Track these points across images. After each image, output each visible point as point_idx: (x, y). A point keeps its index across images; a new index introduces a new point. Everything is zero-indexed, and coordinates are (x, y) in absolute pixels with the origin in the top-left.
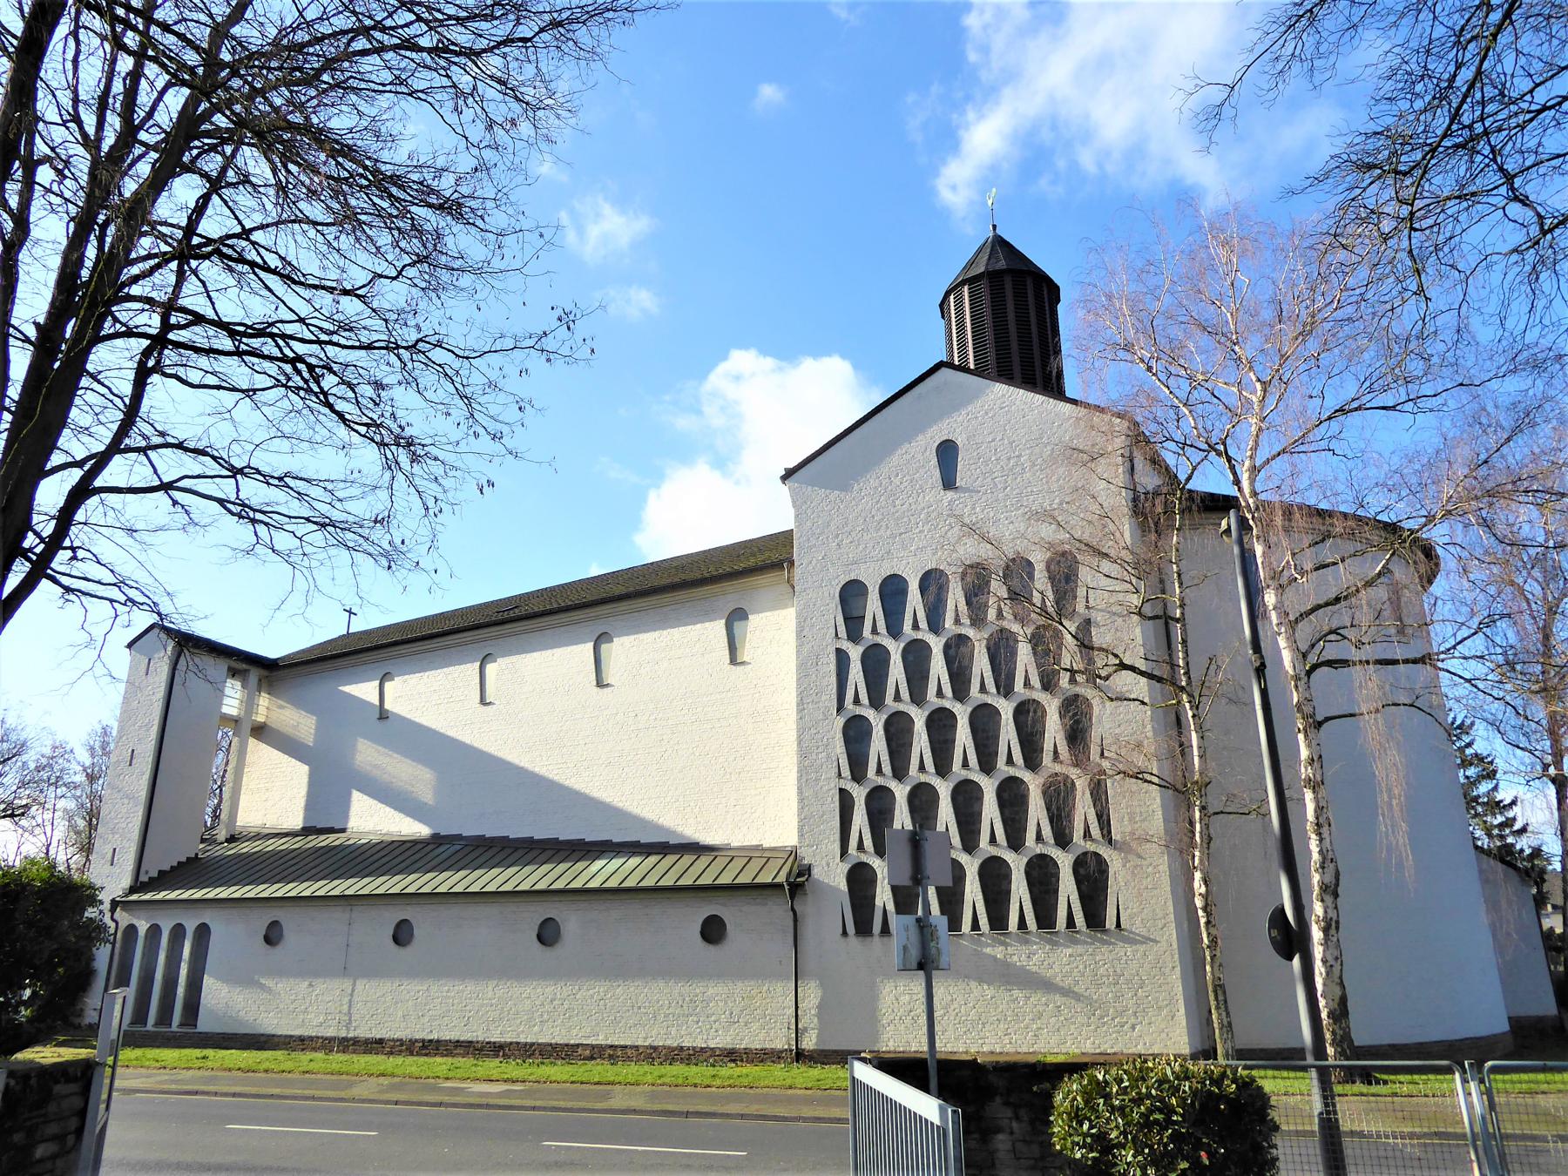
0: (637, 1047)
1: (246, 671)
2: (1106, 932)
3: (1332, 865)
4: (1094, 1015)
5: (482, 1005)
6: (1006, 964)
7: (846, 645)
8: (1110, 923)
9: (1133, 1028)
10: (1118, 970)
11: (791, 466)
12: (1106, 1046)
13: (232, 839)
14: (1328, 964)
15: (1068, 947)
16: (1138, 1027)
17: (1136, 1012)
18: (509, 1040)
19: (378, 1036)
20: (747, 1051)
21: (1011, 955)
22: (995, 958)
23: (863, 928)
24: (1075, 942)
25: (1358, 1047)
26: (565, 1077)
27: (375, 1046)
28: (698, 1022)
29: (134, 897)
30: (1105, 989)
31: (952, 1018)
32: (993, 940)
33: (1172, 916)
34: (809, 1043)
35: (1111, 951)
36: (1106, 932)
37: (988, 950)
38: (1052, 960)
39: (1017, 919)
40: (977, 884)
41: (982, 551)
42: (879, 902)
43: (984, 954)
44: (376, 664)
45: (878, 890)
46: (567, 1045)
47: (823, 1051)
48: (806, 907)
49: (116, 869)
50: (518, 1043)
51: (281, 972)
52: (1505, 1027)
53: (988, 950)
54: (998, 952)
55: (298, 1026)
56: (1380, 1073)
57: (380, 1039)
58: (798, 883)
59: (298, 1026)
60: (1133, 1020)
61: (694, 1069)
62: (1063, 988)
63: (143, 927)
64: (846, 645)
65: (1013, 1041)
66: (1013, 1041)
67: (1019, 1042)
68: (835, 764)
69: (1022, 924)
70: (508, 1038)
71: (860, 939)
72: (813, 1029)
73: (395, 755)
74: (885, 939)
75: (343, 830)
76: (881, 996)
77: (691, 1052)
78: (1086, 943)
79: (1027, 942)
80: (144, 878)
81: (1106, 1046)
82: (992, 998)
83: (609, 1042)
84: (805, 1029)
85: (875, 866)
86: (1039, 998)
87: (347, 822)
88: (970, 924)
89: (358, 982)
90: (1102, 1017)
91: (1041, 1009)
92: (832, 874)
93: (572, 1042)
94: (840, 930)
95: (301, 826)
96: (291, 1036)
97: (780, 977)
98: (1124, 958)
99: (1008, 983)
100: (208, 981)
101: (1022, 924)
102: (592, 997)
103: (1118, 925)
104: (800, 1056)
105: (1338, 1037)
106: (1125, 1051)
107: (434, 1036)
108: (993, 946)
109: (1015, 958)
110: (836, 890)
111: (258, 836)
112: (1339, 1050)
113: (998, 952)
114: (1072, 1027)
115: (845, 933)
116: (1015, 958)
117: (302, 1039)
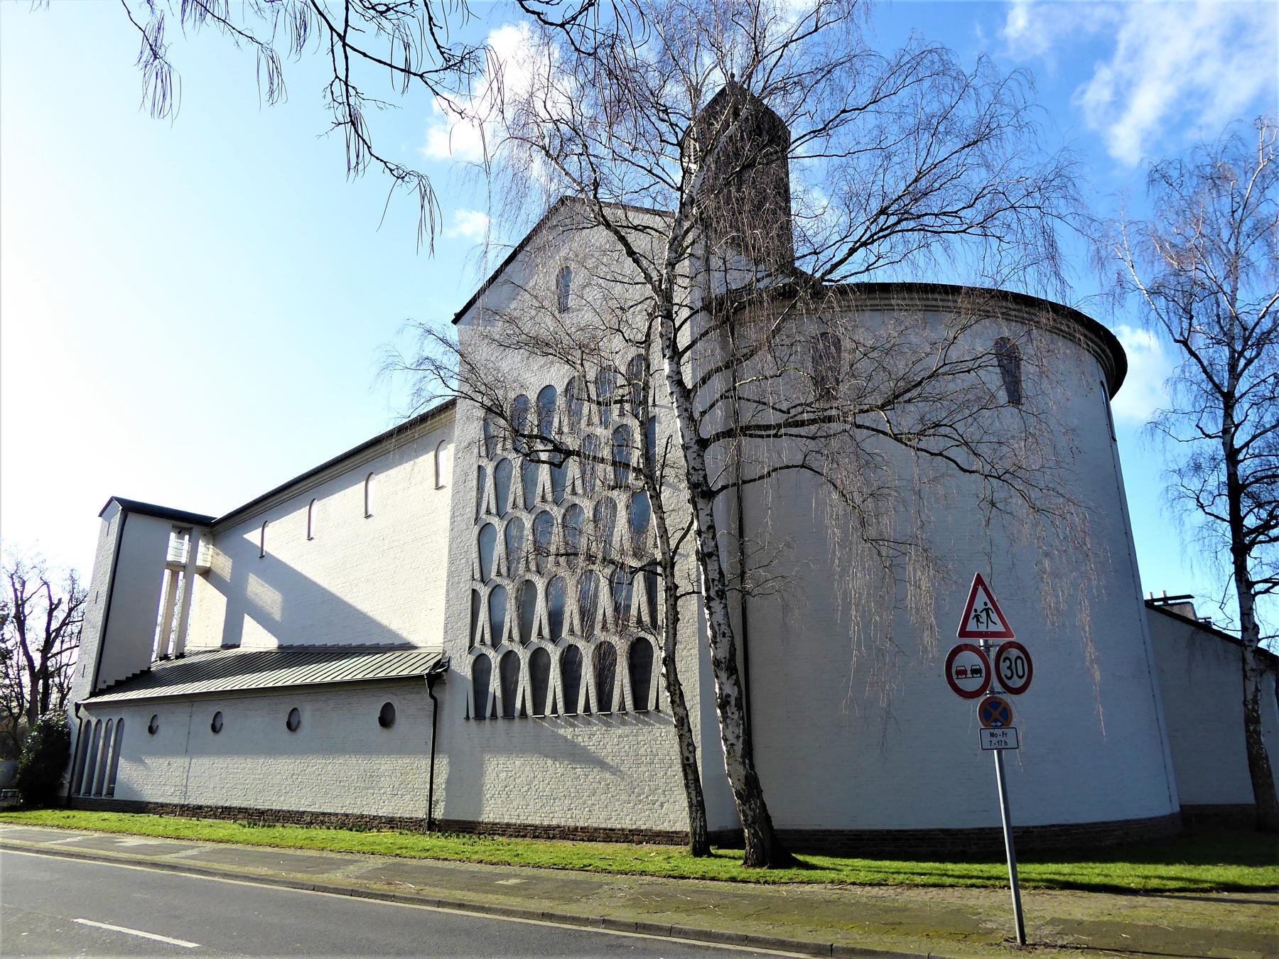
0: (337, 814)
1: (191, 528)
2: (647, 713)
3: (725, 640)
4: (633, 792)
5: (254, 779)
6: (574, 745)
7: (484, 462)
8: (651, 706)
9: (662, 806)
10: (654, 750)
11: (458, 311)
12: (640, 822)
13: (181, 656)
14: (729, 743)
15: (619, 728)
16: (665, 805)
17: (664, 791)
18: (267, 808)
19: (200, 804)
20: (401, 820)
21: (577, 736)
22: (565, 738)
23: (480, 716)
24: (624, 723)
25: (777, 830)
26: (267, 840)
27: (196, 811)
28: (373, 794)
29: (93, 700)
30: (643, 769)
31: (533, 793)
32: (566, 722)
33: (698, 698)
34: (438, 814)
35: (650, 732)
36: (647, 713)
37: (562, 731)
38: (607, 740)
39: (583, 703)
40: (558, 671)
41: (937, 385)
42: (491, 690)
43: (559, 735)
44: (255, 519)
45: (492, 678)
46: (298, 812)
47: (447, 821)
48: (446, 696)
49: (85, 680)
50: (272, 810)
51: (154, 753)
52: (1179, 809)
53: (562, 731)
54: (567, 732)
55: (162, 796)
56: (801, 853)
57: (201, 806)
58: (437, 676)
59: (162, 796)
60: (662, 799)
61: (364, 834)
62: (612, 767)
63: (94, 721)
64: (484, 462)
65: (574, 816)
66: (574, 816)
67: (578, 817)
68: (471, 567)
69: (587, 708)
70: (266, 806)
71: (477, 722)
72: (443, 801)
73: (267, 585)
74: (494, 722)
75: (238, 646)
76: (487, 773)
77: (368, 819)
78: (632, 724)
79: (589, 723)
80: (101, 686)
81: (640, 822)
82: (562, 775)
83: (321, 810)
84: (437, 801)
85: (491, 657)
86: (595, 774)
87: (240, 639)
88: (550, 708)
89: (193, 761)
90: (639, 795)
91: (595, 785)
92: (463, 667)
93: (301, 810)
94: (465, 716)
95: (276, 646)
96: (157, 803)
97: (424, 753)
98: (660, 739)
99: (574, 761)
100: (121, 761)
101: (587, 708)
102: (314, 772)
103: (657, 707)
104: (432, 825)
105: (749, 818)
106: (654, 828)
107: (227, 804)
108: (566, 728)
109: (580, 739)
110: (464, 678)
111: (198, 653)
112: (752, 831)
113: (567, 732)
114: (617, 804)
115: (468, 718)
116: (580, 739)
117: (163, 805)
